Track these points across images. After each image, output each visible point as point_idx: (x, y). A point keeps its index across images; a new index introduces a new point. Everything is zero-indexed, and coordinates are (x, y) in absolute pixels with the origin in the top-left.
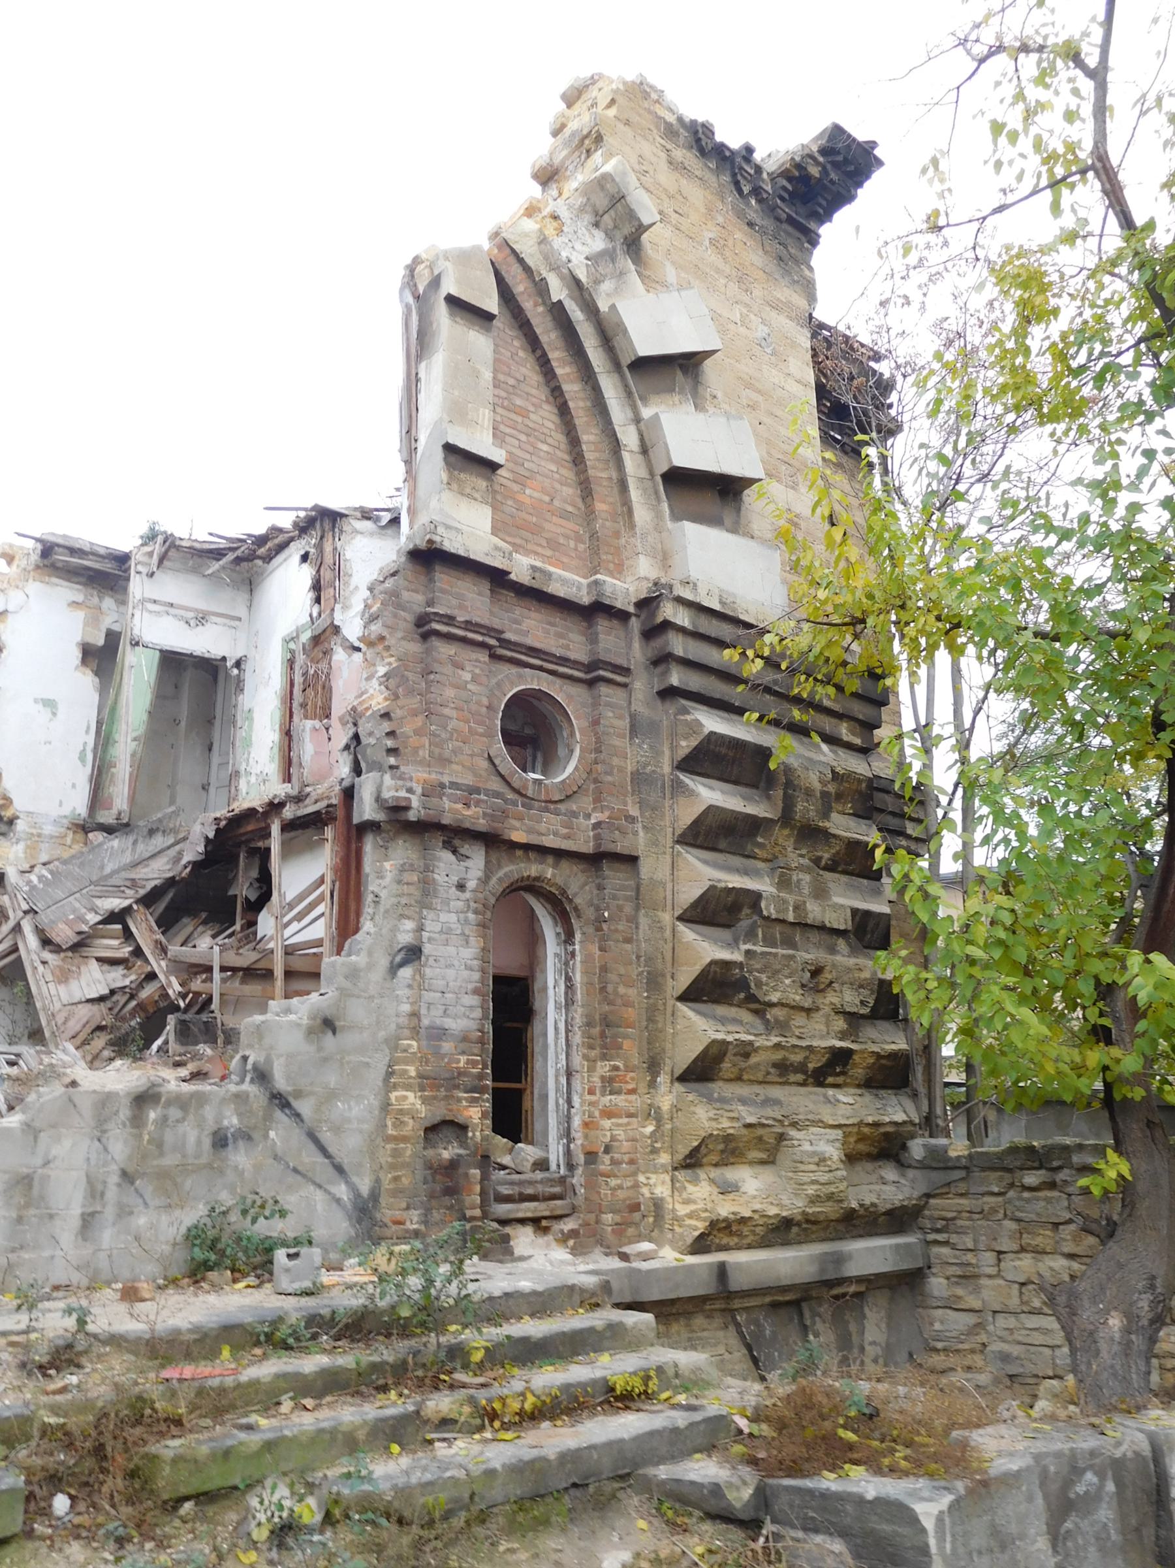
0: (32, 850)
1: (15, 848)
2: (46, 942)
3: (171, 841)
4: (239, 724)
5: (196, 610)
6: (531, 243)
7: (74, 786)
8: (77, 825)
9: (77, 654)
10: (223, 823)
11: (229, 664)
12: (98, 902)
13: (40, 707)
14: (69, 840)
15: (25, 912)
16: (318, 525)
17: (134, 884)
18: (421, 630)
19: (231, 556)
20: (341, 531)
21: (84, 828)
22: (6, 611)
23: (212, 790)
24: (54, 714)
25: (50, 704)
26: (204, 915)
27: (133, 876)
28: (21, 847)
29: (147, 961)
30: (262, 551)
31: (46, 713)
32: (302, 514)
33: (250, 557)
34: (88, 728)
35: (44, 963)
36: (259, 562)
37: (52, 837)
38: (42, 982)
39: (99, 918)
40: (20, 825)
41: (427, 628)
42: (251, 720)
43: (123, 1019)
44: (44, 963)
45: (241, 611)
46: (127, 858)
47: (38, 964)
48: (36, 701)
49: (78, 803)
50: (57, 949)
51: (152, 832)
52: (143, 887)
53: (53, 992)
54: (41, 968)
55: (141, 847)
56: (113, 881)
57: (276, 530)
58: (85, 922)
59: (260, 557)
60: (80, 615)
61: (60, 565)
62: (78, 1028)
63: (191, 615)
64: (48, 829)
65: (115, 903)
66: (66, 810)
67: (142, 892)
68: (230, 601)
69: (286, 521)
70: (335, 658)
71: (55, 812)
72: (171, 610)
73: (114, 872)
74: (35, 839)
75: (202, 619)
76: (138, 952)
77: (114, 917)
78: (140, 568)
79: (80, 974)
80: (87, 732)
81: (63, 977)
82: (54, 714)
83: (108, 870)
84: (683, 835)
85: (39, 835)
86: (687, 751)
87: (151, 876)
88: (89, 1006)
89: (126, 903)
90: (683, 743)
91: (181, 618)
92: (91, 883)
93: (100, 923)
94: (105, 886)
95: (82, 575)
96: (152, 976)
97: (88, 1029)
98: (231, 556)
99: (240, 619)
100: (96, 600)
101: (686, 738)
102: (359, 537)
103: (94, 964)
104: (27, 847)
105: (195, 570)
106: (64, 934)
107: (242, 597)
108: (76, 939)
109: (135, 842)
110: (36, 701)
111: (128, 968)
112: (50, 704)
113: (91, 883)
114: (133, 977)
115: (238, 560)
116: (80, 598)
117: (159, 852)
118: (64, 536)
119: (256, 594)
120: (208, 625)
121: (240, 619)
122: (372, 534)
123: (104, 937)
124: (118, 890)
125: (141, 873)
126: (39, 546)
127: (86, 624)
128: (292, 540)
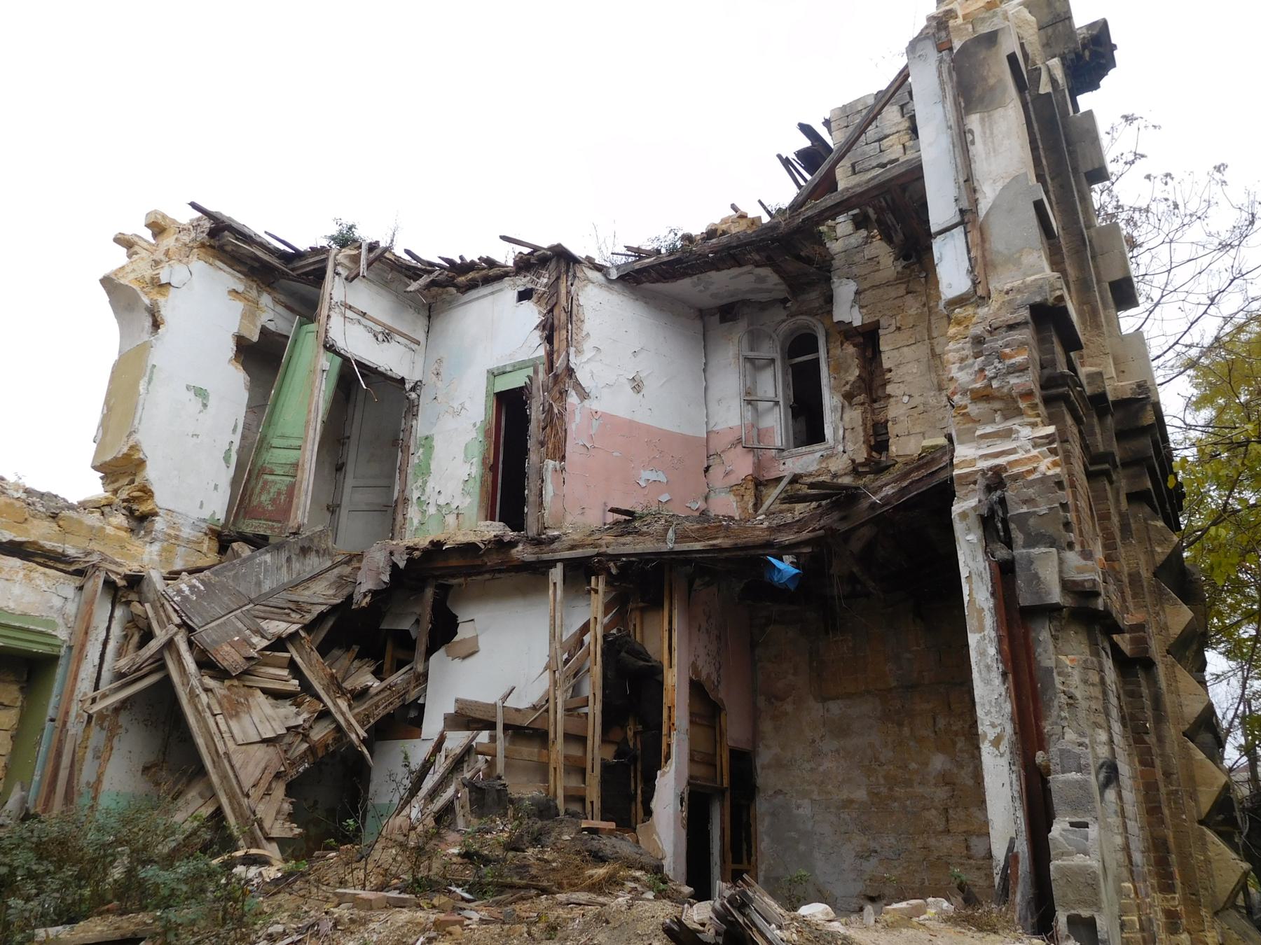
0: (166, 555)
1: (148, 548)
2: (206, 664)
3: (329, 564)
4: (412, 450)
5: (383, 325)
6: (1031, 32)
7: (216, 487)
8: (212, 530)
9: (230, 348)
10: (417, 554)
11: (408, 386)
12: (264, 624)
13: (191, 394)
14: (205, 548)
15: (179, 626)
16: (552, 265)
17: (298, 607)
18: (1044, 392)
19: (425, 280)
20: (575, 276)
21: (223, 540)
22: (169, 284)
23: (344, 512)
24: (205, 405)
25: (201, 393)
26: (356, 648)
27: (295, 598)
28: (156, 547)
29: (319, 699)
30: (462, 279)
31: (196, 403)
32: (526, 250)
33: (450, 282)
34: (236, 426)
35: (207, 690)
36: (453, 290)
37: (189, 541)
38: (208, 714)
39: (265, 643)
40: (159, 524)
41: (1054, 391)
42: (430, 449)
43: (293, 764)
44: (207, 690)
45: (420, 336)
46: (285, 577)
47: (199, 691)
48: (188, 388)
49: (216, 506)
50: (221, 674)
51: (305, 551)
52: (309, 612)
53: (223, 727)
54: (204, 698)
55: (296, 565)
56: (273, 602)
57: (491, 263)
58: (253, 646)
59: (455, 286)
60: (239, 306)
61: (229, 248)
62: (257, 774)
63: (379, 329)
64: (186, 532)
65: (279, 627)
66: (206, 514)
67: (309, 618)
68: (412, 325)
69: (506, 255)
70: (570, 400)
71: (196, 514)
72: (363, 320)
73: (273, 592)
74: (173, 540)
75: (387, 335)
76: (306, 687)
77: (279, 644)
78: (339, 269)
79: (249, 707)
80: (234, 431)
81: (234, 709)
82: (205, 405)
83: (267, 587)
84: (1171, 646)
85: (177, 537)
86: (1163, 558)
87: (315, 600)
88: (263, 747)
89: (294, 628)
90: (1159, 549)
91: (370, 330)
92: (251, 601)
93: (266, 648)
94: (268, 606)
95: (245, 264)
96: (325, 714)
97: (268, 776)
98: (425, 280)
99: (418, 343)
100: (254, 293)
101: (1159, 545)
102: (591, 285)
103: (261, 697)
104: (164, 549)
105: (385, 284)
106: (229, 657)
107: (422, 322)
108: (244, 665)
109: (289, 560)
110: (188, 388)
111: (298, 705)
112: (201, 393)
113: (251, 601)
114: (305, 716)
115: (433, 283)
116: (240, 288)
117: (319, 574)
118: (229, 218)
119: (438, 324)
120: (393, 343)
121: (418, 343)
122: (601, 285)
123: (266, 665)
124: (281, 612)
125: (303, 595)
126: (207, 224)
127: (243, 316)
128: (506, 274)
